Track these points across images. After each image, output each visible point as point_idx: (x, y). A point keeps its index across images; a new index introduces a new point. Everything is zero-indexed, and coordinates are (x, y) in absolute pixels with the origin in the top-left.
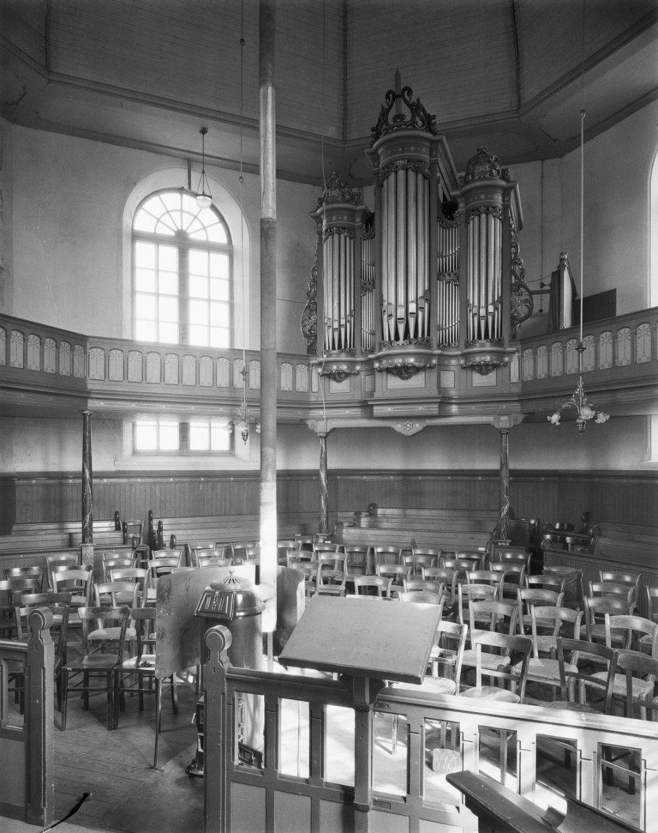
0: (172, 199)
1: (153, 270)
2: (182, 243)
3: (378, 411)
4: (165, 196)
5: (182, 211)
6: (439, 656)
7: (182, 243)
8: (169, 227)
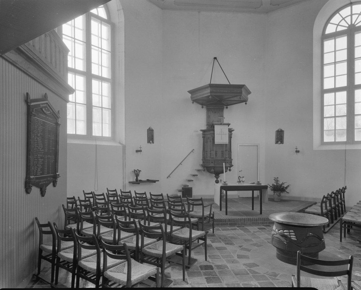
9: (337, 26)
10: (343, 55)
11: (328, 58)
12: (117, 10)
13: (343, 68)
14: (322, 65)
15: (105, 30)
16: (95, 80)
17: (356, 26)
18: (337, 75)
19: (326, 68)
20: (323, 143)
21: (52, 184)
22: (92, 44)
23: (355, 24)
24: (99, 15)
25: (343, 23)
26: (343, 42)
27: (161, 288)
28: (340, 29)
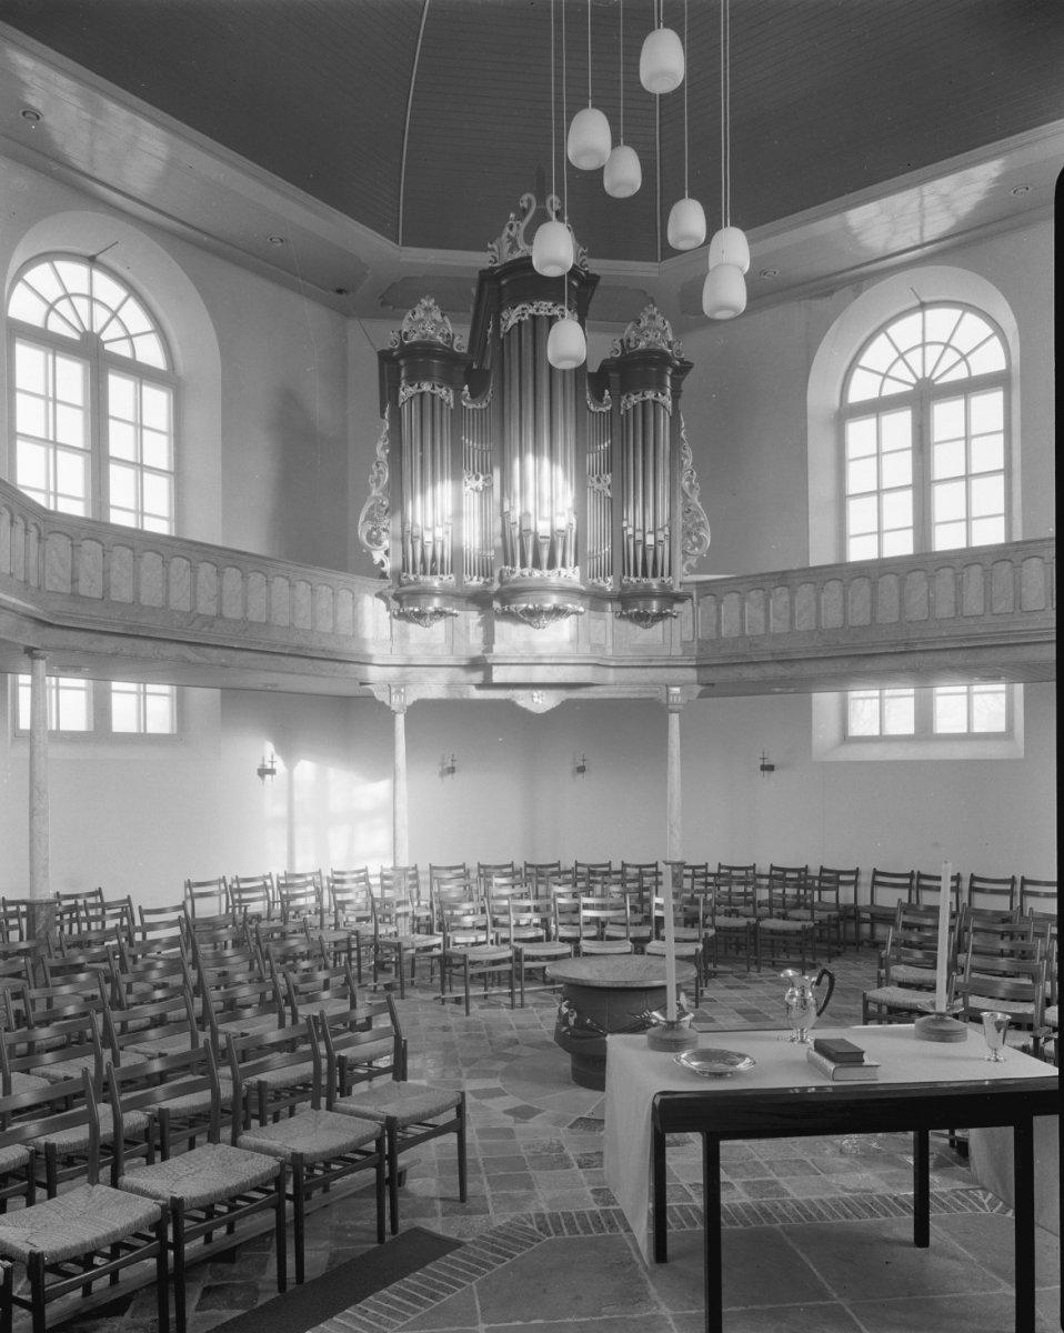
0: (75, 275)
1: (886, 334)
2: (91, 351)
3: (499, 675)
4: (61, 265)
5: (885, 376)
6: (563, 221)
7: (91, 351)
8: (935, 367)
9: (899, 352)
10: (900, 469)
11: (859, 477)
12: (259, 770)
13: (945, 461)
14: (841, 499)
15: (157, 403)
16: (67, 358)
17: (937, 383)
18: (974, 431)
19: (854, 507)
20: (845, 738)
21: (321, 1189)
22: (111, 414)
23: (934, 378)
24: (140, 358)
25: (900, 371)
26: (899, 425)
27: (1060, 896)
28: (892, 388)
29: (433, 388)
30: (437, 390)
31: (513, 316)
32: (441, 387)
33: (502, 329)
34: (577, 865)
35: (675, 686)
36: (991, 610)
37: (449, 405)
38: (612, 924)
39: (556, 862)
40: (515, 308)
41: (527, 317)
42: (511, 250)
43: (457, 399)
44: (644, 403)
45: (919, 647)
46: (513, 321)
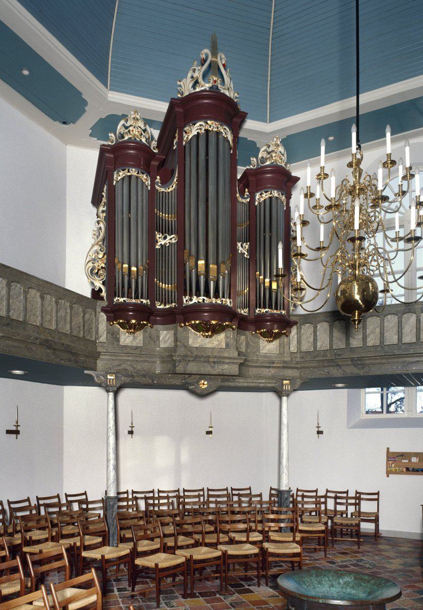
29: (138, 173)
30: (140, 175)
31: (193, 131)
32: (143, 174)
33: (185, 139)
34: (327, 491)
35: (286, 380)
36: (401, 341)
37: (147, 187)
38: (232, 532)
39: (259, 493)
40: (195, 124)
41: (203, 131)
42: (194, 87)
43: (153, 184)
44: (270, 198)
45: (348, 359)
46: (194, 132)
